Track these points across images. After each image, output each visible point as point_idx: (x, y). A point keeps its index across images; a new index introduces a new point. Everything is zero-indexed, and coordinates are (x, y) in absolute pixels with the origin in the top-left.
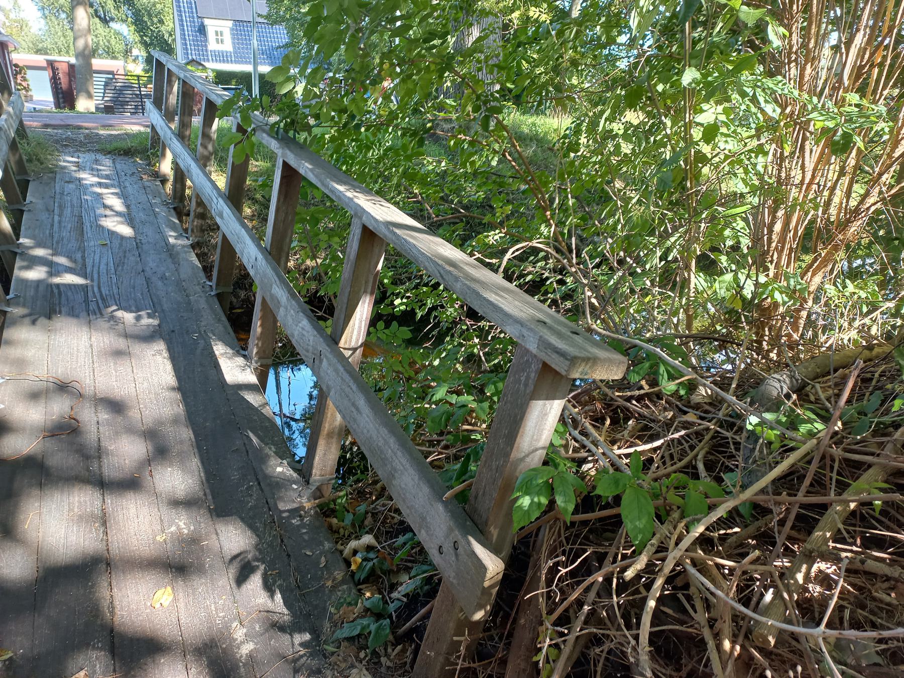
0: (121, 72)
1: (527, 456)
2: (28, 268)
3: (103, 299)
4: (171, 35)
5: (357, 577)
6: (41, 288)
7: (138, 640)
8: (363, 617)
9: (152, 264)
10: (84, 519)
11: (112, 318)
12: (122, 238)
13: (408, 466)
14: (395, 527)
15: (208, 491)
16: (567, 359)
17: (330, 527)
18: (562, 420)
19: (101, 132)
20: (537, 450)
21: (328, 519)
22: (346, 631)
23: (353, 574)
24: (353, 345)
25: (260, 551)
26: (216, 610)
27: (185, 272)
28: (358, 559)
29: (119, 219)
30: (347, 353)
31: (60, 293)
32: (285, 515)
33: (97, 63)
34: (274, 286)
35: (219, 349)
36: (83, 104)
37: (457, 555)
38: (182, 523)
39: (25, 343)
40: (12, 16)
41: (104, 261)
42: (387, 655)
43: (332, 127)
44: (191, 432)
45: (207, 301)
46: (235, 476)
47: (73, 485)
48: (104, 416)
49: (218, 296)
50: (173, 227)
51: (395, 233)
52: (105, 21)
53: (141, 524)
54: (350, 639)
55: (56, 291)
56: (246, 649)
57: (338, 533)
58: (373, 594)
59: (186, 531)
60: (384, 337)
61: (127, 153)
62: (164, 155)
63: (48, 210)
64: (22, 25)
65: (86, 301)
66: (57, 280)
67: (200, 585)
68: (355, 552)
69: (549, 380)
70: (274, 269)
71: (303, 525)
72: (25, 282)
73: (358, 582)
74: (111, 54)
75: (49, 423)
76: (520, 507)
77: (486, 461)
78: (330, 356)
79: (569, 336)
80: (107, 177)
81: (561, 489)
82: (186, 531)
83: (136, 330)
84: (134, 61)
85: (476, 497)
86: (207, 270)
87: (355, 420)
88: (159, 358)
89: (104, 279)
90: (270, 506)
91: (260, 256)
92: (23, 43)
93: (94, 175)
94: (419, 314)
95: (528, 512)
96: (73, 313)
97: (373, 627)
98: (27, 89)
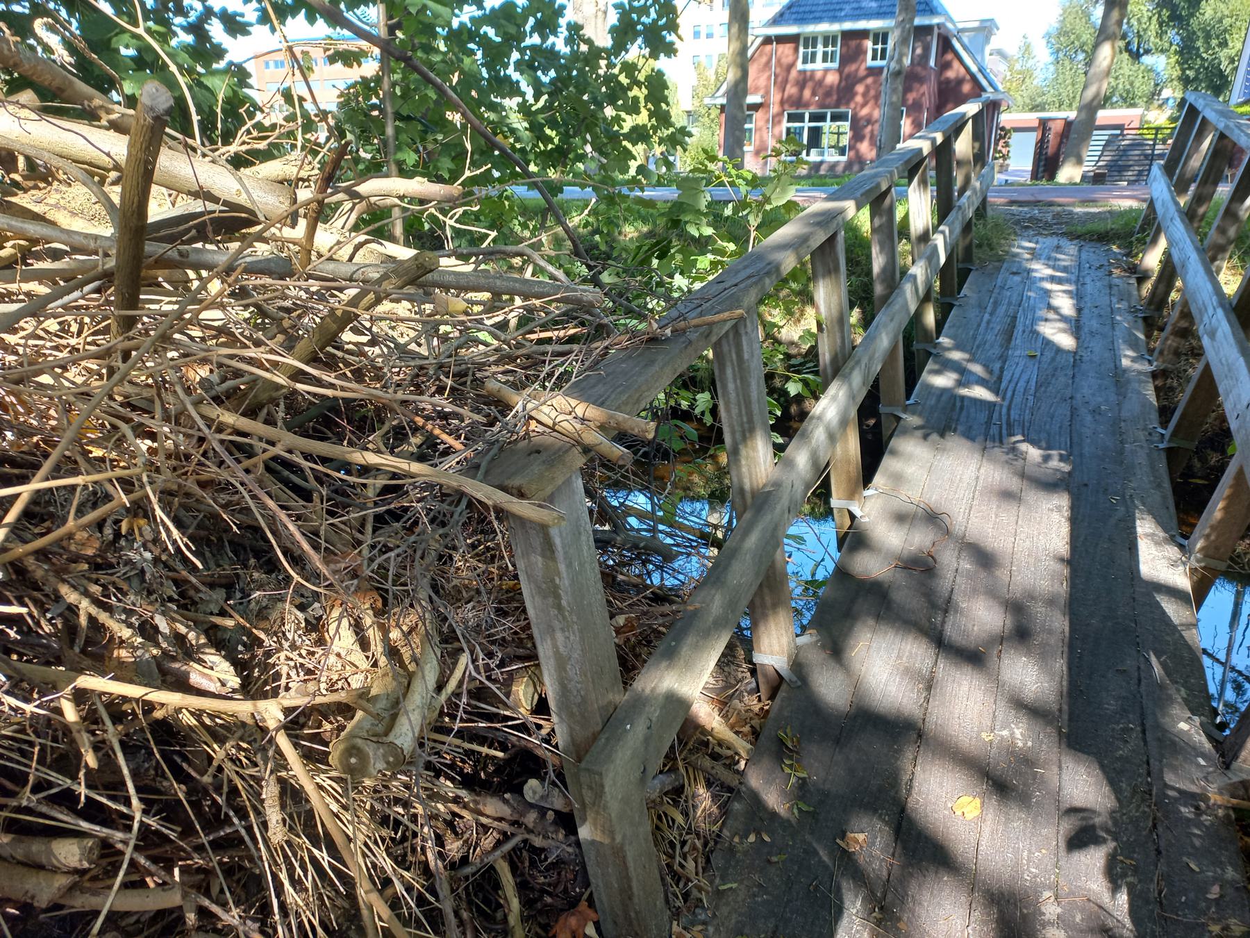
0: (1136, 124)
2: (938, 372)
3: (1009, 424)
6: (944, 398)
7: (926, 837)
9: (1086, 391)
10: (909, 673)
11: (1013, 450)
12: (1059, 350)
15: (1065, 707)
19: (1078, 210)
25: (1116, 822)
26: (1029, 860)
27: (1131, 407)
29: (1061, 325)
31: (962, 408)
32: (1171, 793)
35: (1145, 527)
36: (1068, 173)
38: (1019, 733)
39: (910, 458)
41: (1025, 377)
44: (1067, 623)
45: (1148, 455)
46: (1111, 705)
47: (910, 631)
48: (966, 565)
49: (1169, 451)
50: (1133, 344)
52: (1136, 56)
53: (970, 709)
55: (958, 404)
59: (1020, 744)
61: (1103, 238)
62: (1154, 241)
63: (980, 306)
66: (964, 392)
67: (1019, 822)
72: (929, 388)
74: (1129, 100)
75: (905, 552)
80: (1065, 269)
82: (1020, 744)
83: (1037, 472)
84: (1160, 106)
86: (1165, 413)
88: (1056, 516)
89: (1018, 399)
93: (1049, 266)
96: (969, 436)
98: (1005, 157)
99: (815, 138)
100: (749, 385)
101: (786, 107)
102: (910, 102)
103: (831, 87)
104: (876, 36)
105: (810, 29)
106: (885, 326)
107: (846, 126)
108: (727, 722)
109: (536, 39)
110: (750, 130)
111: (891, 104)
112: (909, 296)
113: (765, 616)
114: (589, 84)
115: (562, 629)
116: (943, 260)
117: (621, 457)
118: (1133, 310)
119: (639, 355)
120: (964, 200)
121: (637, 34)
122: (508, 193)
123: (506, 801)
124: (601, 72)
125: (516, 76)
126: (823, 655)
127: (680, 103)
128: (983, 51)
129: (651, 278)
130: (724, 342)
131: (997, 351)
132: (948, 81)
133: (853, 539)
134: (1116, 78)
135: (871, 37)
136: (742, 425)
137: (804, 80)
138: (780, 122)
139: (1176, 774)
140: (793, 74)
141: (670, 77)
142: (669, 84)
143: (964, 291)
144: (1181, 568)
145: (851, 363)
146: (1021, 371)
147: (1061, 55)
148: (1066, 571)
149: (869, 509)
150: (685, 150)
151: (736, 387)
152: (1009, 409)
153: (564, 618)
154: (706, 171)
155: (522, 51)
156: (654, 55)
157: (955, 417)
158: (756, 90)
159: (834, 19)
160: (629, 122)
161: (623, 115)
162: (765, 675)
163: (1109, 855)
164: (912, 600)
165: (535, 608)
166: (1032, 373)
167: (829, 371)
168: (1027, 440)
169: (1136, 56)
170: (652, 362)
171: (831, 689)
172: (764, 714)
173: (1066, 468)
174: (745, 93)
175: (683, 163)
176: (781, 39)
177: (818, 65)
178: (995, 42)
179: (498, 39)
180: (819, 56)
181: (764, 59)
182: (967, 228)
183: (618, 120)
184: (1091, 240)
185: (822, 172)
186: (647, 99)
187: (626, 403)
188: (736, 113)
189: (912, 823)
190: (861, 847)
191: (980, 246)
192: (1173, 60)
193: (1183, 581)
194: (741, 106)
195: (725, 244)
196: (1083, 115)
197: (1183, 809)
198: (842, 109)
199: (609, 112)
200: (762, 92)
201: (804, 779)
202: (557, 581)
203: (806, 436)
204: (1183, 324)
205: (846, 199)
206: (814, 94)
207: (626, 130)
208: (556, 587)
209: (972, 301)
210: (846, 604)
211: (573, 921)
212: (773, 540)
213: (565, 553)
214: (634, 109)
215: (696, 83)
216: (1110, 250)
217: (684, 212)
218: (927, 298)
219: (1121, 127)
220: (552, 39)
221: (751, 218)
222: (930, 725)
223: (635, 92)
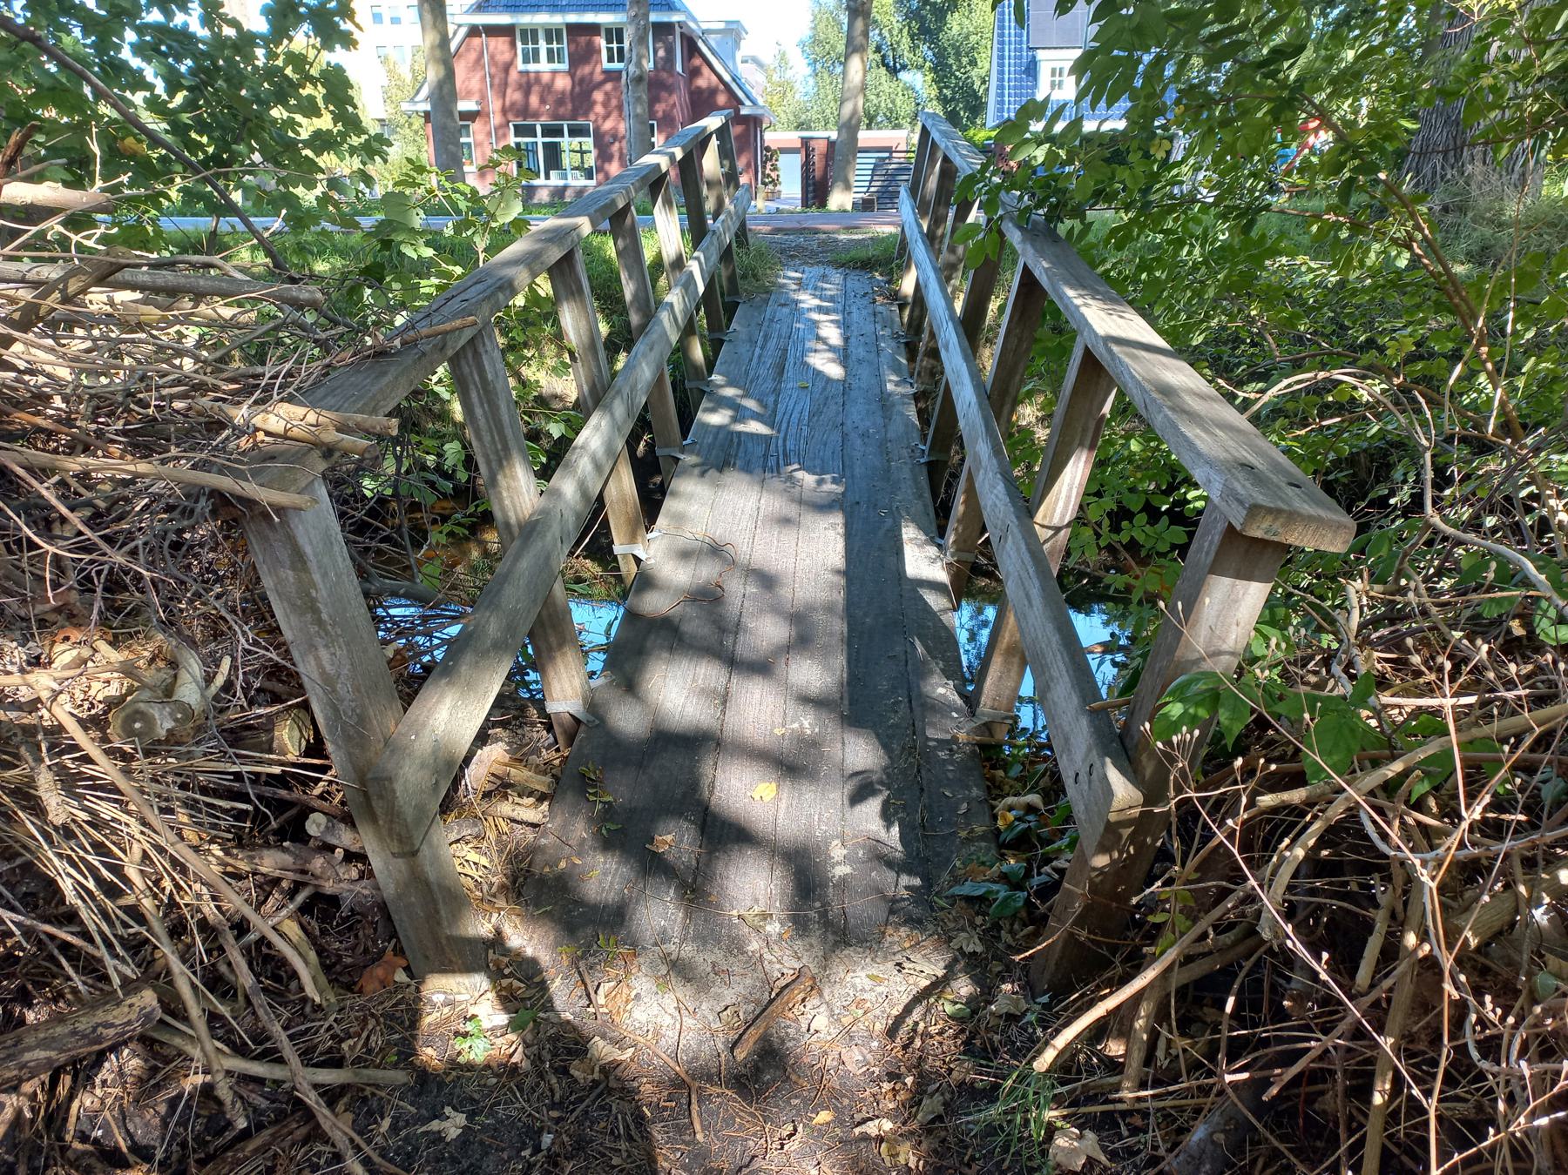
0: (903, 147)
2: (713, 410)
3: (785, 455)
4: (984, 82)
8: (994, 882)
10: (706, 693)
11: (790, 478)
12: (829, 380)
17: (992, 779)
19: (842, 237)
20: (1220, 653)
22: (967, 889)
23: (998, 832)
24: (1056, 521)
25: (888, 776)
27: (896, 428)
28: (1011, 816)
29: (830, 355)
33: (865, 137)
35: (909, 532)
36: (839, 200)
38: (807, 722)
39: (691, 497)
40: (775, 78)
41: (798, 408)
42: (1012, 932)
45: (912, 470)
46: (884, 686)
48: (752, 589)
49: (929, 464)
50: (897, 369)
51: (1110, 351)
52: (893, 71)
53: (761, 711)
54: (969, 899)
56: (841, 871)
61: (866, 265)
62: (908, 267)
64: (785, 88)
65: (766, 456)
66: (740, 427)
68: (1010, 809)
72: (705, 426)
73: (1004, 846)
76: (1166, 715)
78: (1016, 530)
80: (832, 299)
83: (818, 498)
88: (831, 533)
89: (792, 430)
90: (914, 728)
92: (783, 115)
93: (815, 296)
96: (747, 469)
97: (1002, 894)
98: (775, 182)
99: (553, 157)
100: (498, 408)
101: (510, 117)
102: (660, 114)
103: (563, 93)
104: (609, 31)
105: (526, 19)
106: (644, 355)
107: (588, 143)
110: (469, 145)
114: (246, 78)
115: (326, 646)
116: (701, 289)
118: (895, 337)
121: (301, 19)
123: (285, 850)
124: (260, 63)
125: (135, 62)
127: (371, 107)
129: (366, 317)
130: (463, 362)
131: (770, 385)
132: (699, 90)
134: (878, 95)
135: (603, 33)
137: (528, 84)
138: (505, 136)
141: (351, 74)
142: (352, 80)
143: (734, 325)
145: (611, 393)
146: (795, 403)
147: (819, 66)
148: (843, 582)
149: (653, 550)
150: (385, 161)
155: (140, 30)
156: (327, 45)
157: (733, 452)
159: (555, 8)
160: (307, 127)
161: (298, 118)
162: (561, 725)
164: (703, 629)
165: (291, 628)
166: (806, 404)
167: (590, 403)
169: (893, 71)
170: (384, 373)
174: (453, 96)
175: (385, 177)
176: (493, 31)
177: (544, 66)
178: (746, 48)
179: (103, 13)
181: (473, 56)
182: (726, 255)
185: (568, 200)
186: (326, 99)
188: (446, 122)
191: (744, 277)
192: (929, 78)
194: (450, 113)
196: (844, 135)
199: (277, 113)
200: (476, 97)
201: (609, 803)
206: (543, 101)
208: (313, 600)
209: (743, 336)
211: (379, 972)
214: (311, 110)
215: (386, 83)
217: (394, 230)
218: (689, 330)
219: (889, 150)
221: (477, 239)
223: (308, 90)
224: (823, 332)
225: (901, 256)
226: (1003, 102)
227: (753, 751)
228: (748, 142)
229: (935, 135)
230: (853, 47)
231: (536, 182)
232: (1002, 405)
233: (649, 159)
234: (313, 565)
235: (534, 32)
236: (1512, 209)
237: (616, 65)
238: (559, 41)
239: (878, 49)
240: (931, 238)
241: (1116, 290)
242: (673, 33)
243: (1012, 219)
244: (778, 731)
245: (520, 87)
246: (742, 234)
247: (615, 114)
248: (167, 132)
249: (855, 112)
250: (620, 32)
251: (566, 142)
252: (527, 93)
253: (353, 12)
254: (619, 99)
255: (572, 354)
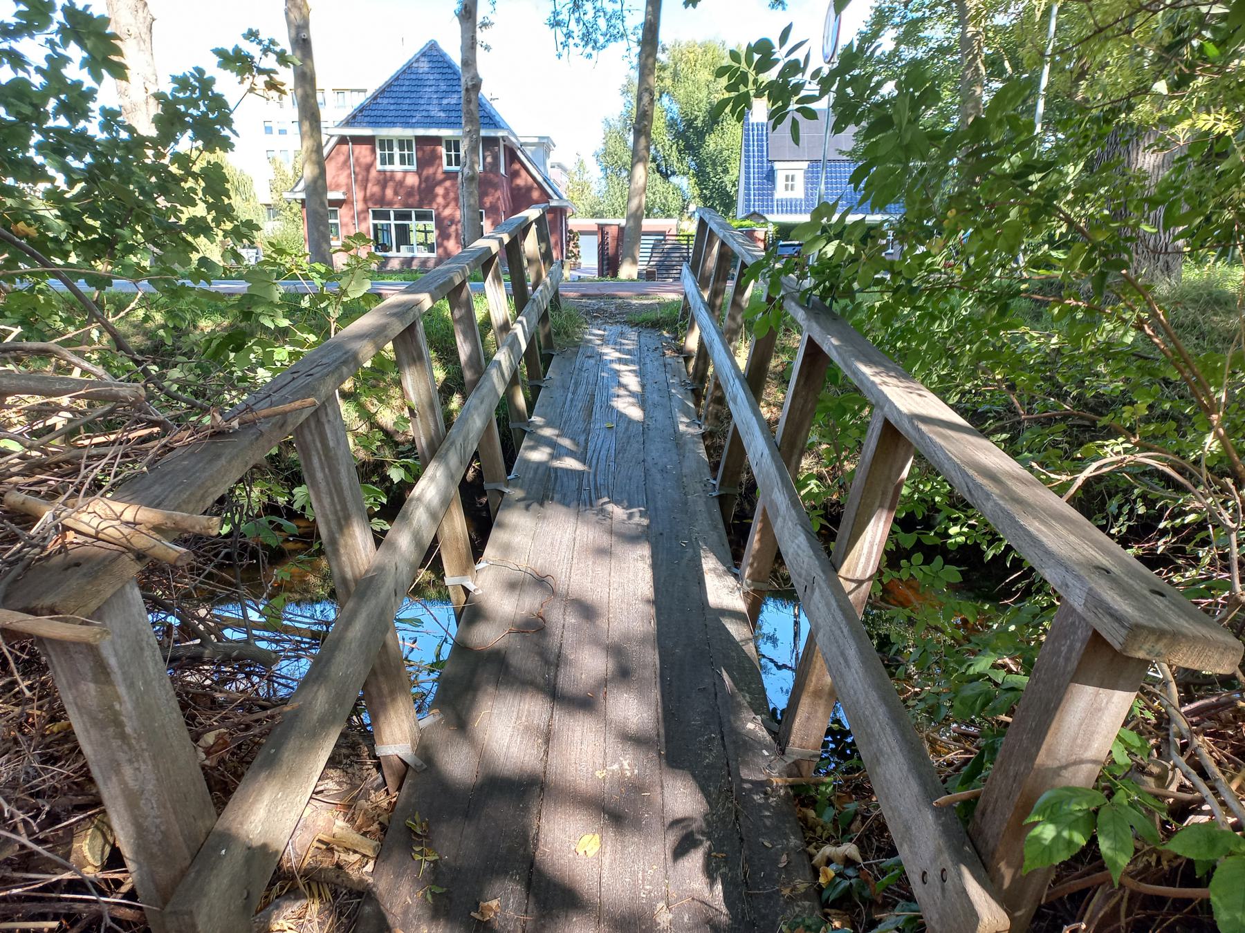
0: (674, 232)
1: (1065, 767)
2: (533, 448)
3: (596, 489)
4: (734, 185)
5: (825, 895)
6: (540, 471)
7: (555, 885)
9: (655, 454)
11: (602, 511)
12: (630, 421)
13: (897, 749)
14: (877, 839)
15: (662, 731)
16: (1123, 626)
17: (804, 819)
18: (1129, 721)
19: (634, 302)
20: (1081, 762)
21: (804, 810)
23: (820, 890)
25: (708, 824)
26: (643, 880)
27: (689, 465)
28: (831, 871)
29: (631, 400)
30: (849, 586)
31: (556, 477)
32: (746, 786)
33: (648, 224)
34: (776, 490)
35: (709, 564)
36: (627, 271)
37: (943, 889)
38: (626, 764)
39: (514, 528)
41: (606, 446)
43: (882, 292)
44: (657, 656)
45: (706, 503)
46: (697, 721)
47: (527, 691)
48: (572, 619)
49: (720, 497)
50: (686, 413)
51: (919, 430)
52: (666, 176)
53: (590, 753)
55: (553, 475)
57: (815, 832)
58: (843, 926)
59: (629, 774)
60: (919, 576)
61: (656, 325)
62: (692, 328)
63: (563, 387)
64: (583, 188)
65: (579, 490)
66: (557, 464)
67: (633, 843)
68: (829, 861)
69: (1107, 661)
70: (779, 469)
71: (766, 806)
72: (527, 462)
74: (666, 212)
75: (518, 617)
76: (1038, 839)
77: (1002, 763)
78: (824, 585)
79: (1144, 597)
80: (629, 352)
81: (1111, 828)
82: (629, 774)
84: (690, 218)
85: (983, 814)
86: (714, 468)
87: (842, 675)
88: (641, 565)
89: (602, 466)
90: (732, 772)
91: (766, 452)
93: (616, 350)
94: (990, 554)
95: (1049, 850)
96: (565, 502)
98: (576, 256)
99: (403, 236)
100: (338, 473)
101: (370, 205)
102: (488, 205)
103: (412, 187)
104: (448, 143)
106: (476, 408)
107: (431, 225)
108: (353, 826)
109: (62, 122)
110: (336, 225)
111: (469, 206)
112: (496, 382)
113: (383, 706)
115: (130, 761)
116: (524, 347)
117: (180, 558)
118: (683, 384)
119: (203, 451)
120: (537, 294)
121: (185, 127)
122: (42, 285)
125: (39, 160)
126: (447, 732)
128: (545, 164)
129: (232, 373)
130: (306, 432)
131: (581, 425)
132: (519, 188)
133: (471, 613)
135: (444, 144)
136: (336, 512)
137: (385, 180)
138: (365, 219)
139: (749, 769)
140: (373, 173)
144: (737, 593)
145: (446, 445)
146: (601, 440)
148: (653, 611)
149: (484, 582)
151: (325, 476)
152: (595, 476)
153: (130, 747)
154: (275, 264)
155: (46, 133)
156: (209, 147)
158: (337, 187)
159: (407, 125)
162: (390, 767)
163: (705, 853)
164: (526, 663)
165: (91, 743)
167: (427, 454)
168: (614, 501)
169: (666, 176)
170: (219, 456)
171: (458, 764)
172: (392, 805)
173: (645, 522)
176: (357, 140)
177: (397, 167)
178: (554, 157)
180: (397, 159)
181: (341, 158)
182: (544, 318)
183: (174, 211)
184: (647, 327)
187: (187, 502)
188: (318, 209)
189: (540, 873)
190: (496, 914)
191: (557, 334)
192: (693, 181)
193: (740, 605)
194: (322, 204)
195: (305, 336)
196: (631, 223)
197: (756, 797)
198: (425, 209)
199: (162, 202)
200: (344, 189)
201: (435, 862)
202: (117, 707)
203: (407, 518)
204: (718, 394)
205: (421, 292)
206: (396, 193)
207: (183, 222)
208: (116, 714)
210: (468, 676)
212: (383, 624)
213: (123, 673)
216: (661, 335)
217: (257, 304)
218: (514, 381)
219: (663, 233)
220: (82, 124)
221: (330, 310)
222: (551, 777)
224: (626, 384)
225: (683, 318)
226: (749, 200)
227: (574, 797)
228: (556, 226)
229: (712, 225)
230: (637, 158)
231: (389, 254)
232: (791, 456)
233: (480, 243)
234: (117, 676)
235: (390, 142)
236: (1163, 288)
237: (454, 168)
238: (410, 149)
239: (654, 160)
240: (711, 306)
241: (902, 364)
242: (498, 145)
243: (793, 299)
244: (599, 774)
245: (378, 182)
246: (556, 300)
247: (453, 204)
248: (57, 217)
249: (639, 207)
250: (457, 144)
251: (414, 224)
252: (384, 187)
253: (231, 121)
254: (456, 193)
255: (411, 411)
